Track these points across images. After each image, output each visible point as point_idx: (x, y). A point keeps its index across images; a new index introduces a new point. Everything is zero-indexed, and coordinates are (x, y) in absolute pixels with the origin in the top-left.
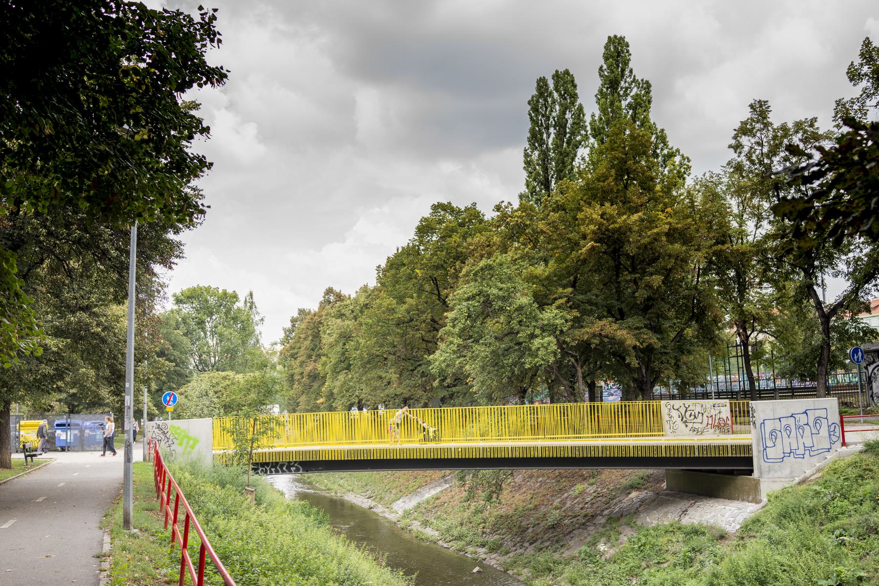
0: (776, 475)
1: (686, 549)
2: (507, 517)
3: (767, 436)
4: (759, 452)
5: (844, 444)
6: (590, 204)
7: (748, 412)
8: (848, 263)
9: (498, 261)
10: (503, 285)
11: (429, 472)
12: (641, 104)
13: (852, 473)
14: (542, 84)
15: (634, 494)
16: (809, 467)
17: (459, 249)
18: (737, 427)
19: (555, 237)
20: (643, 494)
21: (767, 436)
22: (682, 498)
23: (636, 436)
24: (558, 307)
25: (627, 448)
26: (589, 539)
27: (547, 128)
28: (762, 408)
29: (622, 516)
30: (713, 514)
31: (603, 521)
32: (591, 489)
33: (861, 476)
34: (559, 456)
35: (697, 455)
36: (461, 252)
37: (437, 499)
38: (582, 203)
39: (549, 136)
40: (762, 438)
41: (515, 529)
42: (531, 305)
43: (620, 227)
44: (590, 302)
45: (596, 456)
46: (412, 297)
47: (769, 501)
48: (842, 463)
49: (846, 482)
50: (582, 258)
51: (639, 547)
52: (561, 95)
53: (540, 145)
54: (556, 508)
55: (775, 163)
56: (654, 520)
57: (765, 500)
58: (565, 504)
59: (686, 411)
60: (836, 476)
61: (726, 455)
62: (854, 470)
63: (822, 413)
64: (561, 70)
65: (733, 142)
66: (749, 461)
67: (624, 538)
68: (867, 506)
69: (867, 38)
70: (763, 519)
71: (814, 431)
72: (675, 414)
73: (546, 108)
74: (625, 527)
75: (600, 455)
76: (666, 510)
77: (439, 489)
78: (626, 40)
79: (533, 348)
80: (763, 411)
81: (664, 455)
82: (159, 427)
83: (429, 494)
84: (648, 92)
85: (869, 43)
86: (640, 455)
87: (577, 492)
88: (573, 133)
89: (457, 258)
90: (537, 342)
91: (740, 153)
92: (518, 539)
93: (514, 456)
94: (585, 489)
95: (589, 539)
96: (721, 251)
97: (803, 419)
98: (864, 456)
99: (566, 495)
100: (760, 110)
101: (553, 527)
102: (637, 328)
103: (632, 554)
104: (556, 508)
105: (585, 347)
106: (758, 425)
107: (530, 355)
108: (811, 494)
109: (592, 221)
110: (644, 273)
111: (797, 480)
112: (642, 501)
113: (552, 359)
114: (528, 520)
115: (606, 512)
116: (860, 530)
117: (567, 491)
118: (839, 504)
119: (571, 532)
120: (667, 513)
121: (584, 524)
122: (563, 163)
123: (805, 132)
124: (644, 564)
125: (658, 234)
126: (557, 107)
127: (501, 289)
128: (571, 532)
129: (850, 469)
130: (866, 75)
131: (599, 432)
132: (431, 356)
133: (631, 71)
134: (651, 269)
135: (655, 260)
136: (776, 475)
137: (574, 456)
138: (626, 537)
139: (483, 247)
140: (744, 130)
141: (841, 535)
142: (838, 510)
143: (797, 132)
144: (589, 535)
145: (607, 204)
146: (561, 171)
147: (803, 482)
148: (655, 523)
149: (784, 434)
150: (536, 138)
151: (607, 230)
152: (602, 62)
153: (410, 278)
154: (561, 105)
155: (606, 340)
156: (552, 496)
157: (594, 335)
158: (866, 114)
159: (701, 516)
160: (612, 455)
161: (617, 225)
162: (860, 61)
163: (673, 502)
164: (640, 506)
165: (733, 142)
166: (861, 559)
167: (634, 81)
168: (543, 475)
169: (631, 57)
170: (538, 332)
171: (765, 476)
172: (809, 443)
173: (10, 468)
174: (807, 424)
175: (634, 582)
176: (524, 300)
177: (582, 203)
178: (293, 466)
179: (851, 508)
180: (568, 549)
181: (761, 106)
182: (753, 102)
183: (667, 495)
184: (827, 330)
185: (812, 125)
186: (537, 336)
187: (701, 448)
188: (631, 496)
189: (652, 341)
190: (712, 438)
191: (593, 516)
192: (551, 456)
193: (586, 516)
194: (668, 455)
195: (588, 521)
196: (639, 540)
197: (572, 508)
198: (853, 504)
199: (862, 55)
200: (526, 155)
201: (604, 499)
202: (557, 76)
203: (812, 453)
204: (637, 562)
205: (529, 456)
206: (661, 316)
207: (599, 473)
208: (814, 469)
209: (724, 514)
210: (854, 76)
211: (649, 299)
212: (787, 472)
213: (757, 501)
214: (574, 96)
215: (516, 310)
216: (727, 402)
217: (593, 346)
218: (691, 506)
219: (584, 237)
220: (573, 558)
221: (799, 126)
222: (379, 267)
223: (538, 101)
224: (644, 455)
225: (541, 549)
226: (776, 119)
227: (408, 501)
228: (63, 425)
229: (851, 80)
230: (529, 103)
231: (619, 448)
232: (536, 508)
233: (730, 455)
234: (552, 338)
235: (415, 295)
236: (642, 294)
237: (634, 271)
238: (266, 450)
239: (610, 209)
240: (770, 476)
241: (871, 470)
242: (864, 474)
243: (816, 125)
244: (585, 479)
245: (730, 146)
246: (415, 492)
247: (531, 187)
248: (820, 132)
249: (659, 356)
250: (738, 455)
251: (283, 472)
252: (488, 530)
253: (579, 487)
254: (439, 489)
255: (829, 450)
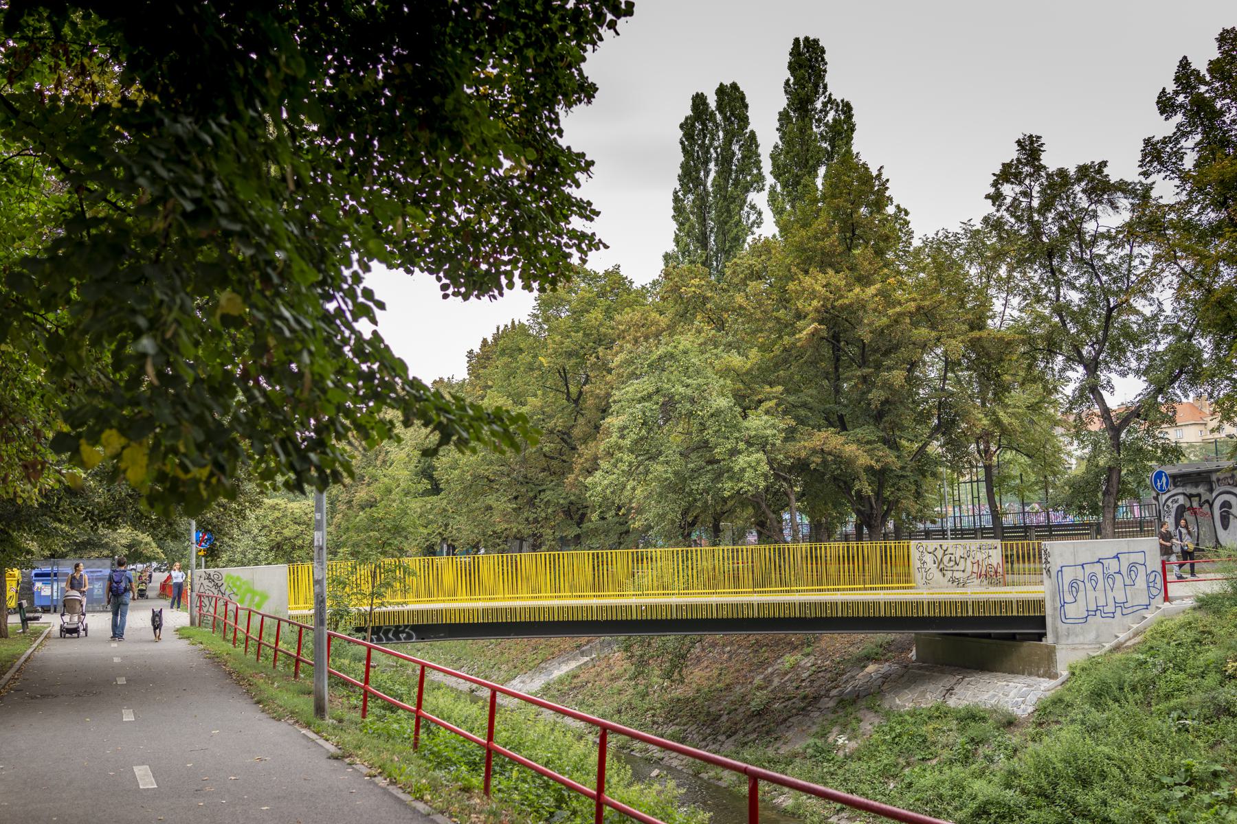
0: (1077, 640)
1: (962, 740)
2: (687, 701)
3: (1066, 587)
4: (1055, 609)
5: (1166, 599)
6: (806, 272)
7: (1040, 554)
8: (1140, 358)
9: (681, 347)
10: (689, 381)
11: (556, 640)
12: (843, 129)
13: (1188, 636)
14: (699, 101)
15: (871, 668)
16: (1122, 630)
17: (602, 330)
18: (1009, 578)
19: (759, 315)
20: (885, 668)
21: (1066, 587)
22: (942, 672)
23: (882, 589)
24: (767, 412)
25: (876, 604)
26: (815, 729)
27: (706, 163)
28: (1060, 551)
29: (858, 696)
30: (991, 693)
31: (831, 704)
32: (807, 662)
33: (1197, 641)
34: (782, 615)
35: (970, 614)
36: (605, 335)
37: (575, 677)
38: (794, 269)
39: (707, 174)
40: (1058, 591)
41: (702, 718)
42: (731, 408)
43: (851, 305)
44: (804, 405)
45: (834, 615)
46: (535, 395)
47: (1073, 674)
48: (1171, 624)
49: (1173, 653)
50: (799, 344)
51: (894, 739)
52: (726, 118)
53: (696, 187)
54: (759, 688)
55: (1050, 220)
56: (905, 701)
57: (1064, 673)
58: (770, 682)
59: (945, 555)
60: (1165, 640)
61: (1009, 614)
62: (1189, 633)
63: (1139, 558)
64: (727, 83)
65: (992, 190)
66: (1041, 621)
67: (866, 727)
68: (1211, 680)
69: (1185, 57)
70: (1067, 698)
71: (1128, 581)
72: (929, 558)
73: (705, 137)
74: (866, 712)
75: (840, 615)
76: (922, 689)
77: (573, 665)
78: (821, 44)
79: (736, 469)
80: (1061, 555)
81: (926, 614)
82: (209, 578)
83: (560, 671)
84: (851, 117)
85: (1188, 64)
86: (893, 615)
87: (787, 665)
88: (741, 171)
89: (599, 341)
90: (741, 461)
91: (1000, 206)
92: (708, 731)
93: (720, 616)
94: (797, 662)
95: (815, 729)
96: (980, 339)
97: (1113, 566)
98: (1198, 614)
99: (770, 670)
100: (1031, 149)
101: (759, 714)
102: (869, 442)
103: (884, 748)
104: (759, 688)
105: (801, 466)
106: (1053, 573)
107: (731, 478)
108: (1132, 665)
109: (813, 295)
110: (878, 366)
111: (1108, 646)
112: (886, 677)
113: (762, 485)
114: (719, 704)
115: (834, 692)
116: (1205, 711)
117: (771, 665)
118: (1174, 677)
119: (785, 720)
120: (923, 694)
121: (803, 709)
122: (728, 211)
123: (1093, 179)
124: (902, 761)
125: (900, 314)
126: (721, 134)
127: (687, 386)
128: (785, 720)
129: (1182, 631)
130: (1181, 106)
131: (820, 583)
132: (590, 479)
133: (825, 87)
134: (887, 362)
135: (895, 348)
136: (1077, 640)
137: (803, 615)
138: (869, 724)
139: (638, 326)
140: (1007, 174)
141: (1180, 718)
142: (1173, 684)
143: (1079, 180)
144: (814, 723)
145: (831, 272)
146: (726, 223)
147: (1117, 648)
148: (909, 706)
149: (1088, 585)
150: (690, 176)
151: (833, 307)
152: (788, 74)
153: (531, 368)
154: (726, 133)
155: (830, 458)
156: (750, 671)
157: (814, 452)
158: (1182, 159)
159: (975, 696)
160: (856, 615)
161: (847, 301)
162: (1174, 87)
163: (930, 679)
164: (883, 683)
165: (992, 190)
166: (1212, 748)
167: (830, 101)
168: (732, 643)
169: (828, 67)
170: (742, 446)
171: (1063, 641)
172: (1120, 598)
173: (6, 637)
174: (1119, 572)
175: (892, 785)
176: (723, 403)
177: (794, 269)
178: (403, 632)
179: (1190, 682)
180: (785, 743)
181: (1032, 143)
182: (1021, 137)
183: (920, 668)
184: (1117, 445)
185: (1100, 171)
186: (740, 453)
187: (931, 604)
188: (867, 670)
189: (889, 460)
190: (977, 592)
191: (816, 699)
192: (771, 615)
193: (805, 697)
194: (932, 614)
195: (809, 704)
196: (892, 729)
197: (782, 687)
198: (1193, 676)
199: (1177, 79)
200: (676, 199)
201: (829, 675)
202: (721, 91)
203: (1125, 611)
204: (893, 758)
205: (740, 616)
206: (896, 426)
207: (817, 640)
208: (1130, 633)
209: (1012, 694)
210: (1165, 106)
211: (887, 401)
212: (1092, 636)
213: (1054, 676)
214: (744, 121)
215: (712, 415)
216: (997, 542)
217: (813, 466)
218: (958, 682)
219: (800, 316)
220: (795, 755)
221: (1083, 171)
222: (471, 352)
223: (693, 125)
224: (899, 614)
225: (746, 743)
226: (1051, 160)
227: (528, 681)
228: (48, 575)
229: (1162, 113)
230: (681, 126)
231: (866, 604)
232: (728, 687)
233: (1015, 614)
234: (760, 455)
235: (539, 393)
236: (876, 396)
237: (864, 363)
238: (390, 608)
239: (838, 280)
240: (1070, 641)
241: (1210, 633)
242: (1203, 637)
243: (1106, 171)
244: (796, 648)
245: (988, 197)
246: (537, 668)
247: (682, 244)
248: (1113, 179)
249: (896, 480)
250: (1026, 614)
251: (388, 639)
252: (661, 720)
253: (789, 659)
254: (573, 665)
255: (1147, 607)
